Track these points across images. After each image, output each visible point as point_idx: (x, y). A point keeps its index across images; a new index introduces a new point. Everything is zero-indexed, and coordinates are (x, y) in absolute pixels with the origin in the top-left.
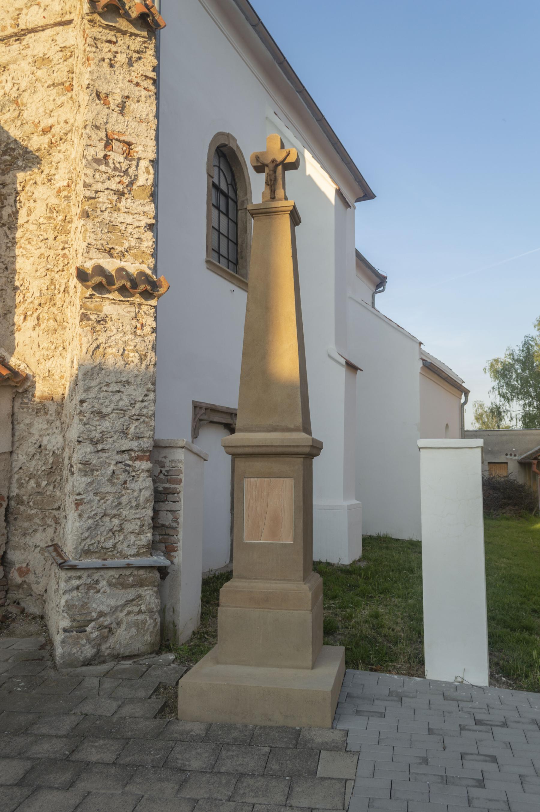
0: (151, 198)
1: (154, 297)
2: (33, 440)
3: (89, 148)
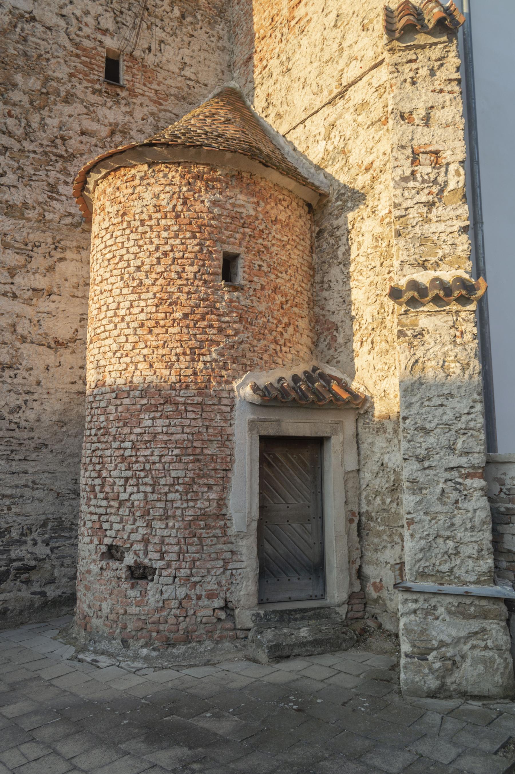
0: (464, 200)
1: (473, 301)
2: (375, 458)
3: (397, 169)
